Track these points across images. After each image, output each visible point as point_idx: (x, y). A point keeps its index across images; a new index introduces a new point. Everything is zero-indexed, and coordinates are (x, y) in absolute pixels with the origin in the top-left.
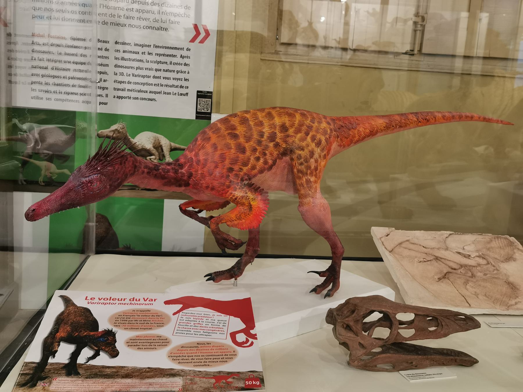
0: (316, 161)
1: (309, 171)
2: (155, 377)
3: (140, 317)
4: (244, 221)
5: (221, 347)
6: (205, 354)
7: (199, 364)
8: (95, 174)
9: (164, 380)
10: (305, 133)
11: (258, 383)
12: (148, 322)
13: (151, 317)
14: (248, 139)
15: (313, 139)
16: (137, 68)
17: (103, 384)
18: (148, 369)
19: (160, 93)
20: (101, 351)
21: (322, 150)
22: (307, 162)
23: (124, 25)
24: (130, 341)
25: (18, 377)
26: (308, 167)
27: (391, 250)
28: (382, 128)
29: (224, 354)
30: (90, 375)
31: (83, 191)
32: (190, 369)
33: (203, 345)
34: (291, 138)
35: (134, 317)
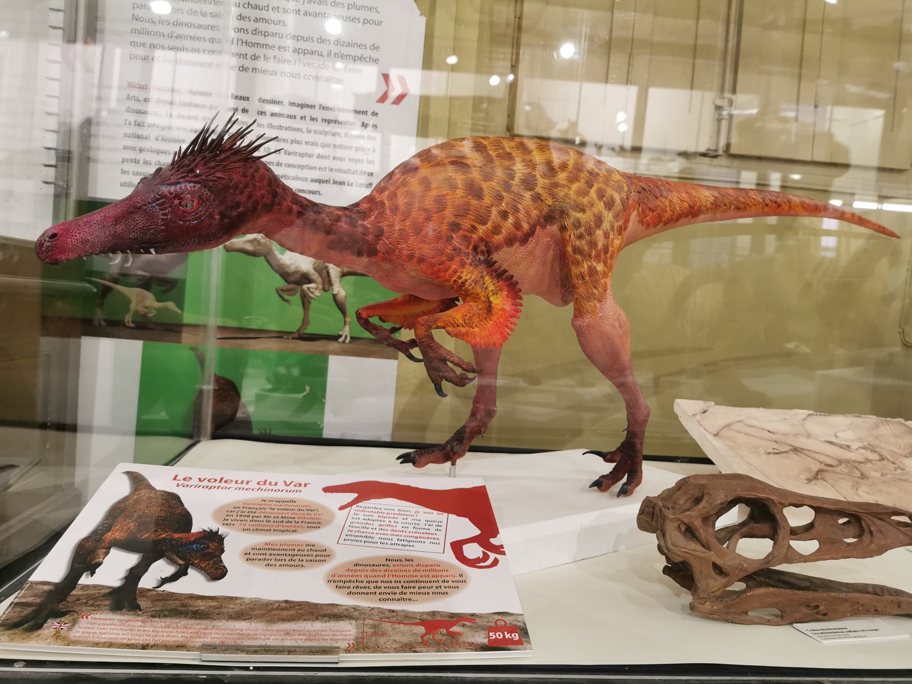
0: (606, 236)
1: (594, 253)
2: (299, 619)
3: (276, 511)
4: (476, 329)
5: (433, 568)
6: (402, 579)
7: (391, 596)
8: (190, 182)
9: (318, 625)
10: (587, 183)
11: (516, 637)
12: (290, 520)
13: (296, 511)
14: (488, 178)
15: (601, 195)
16: (292, 142)
17: (185, 630)
18: (284, 605)
19: (326, 182)
20: (192, 568)
21: (616, 216)
22: (590, 234)
23: (274, 73)
24: (252, 552)
25: (7, 610)
26: (593, 244)
27: (716, 432)
28: (709, 205)
29: (440, 579)
30: (162, 610)
31: (163, 215)
32: (372, 605)
33: (399, 563)
34: (562, 189)
35: (263, 511)
